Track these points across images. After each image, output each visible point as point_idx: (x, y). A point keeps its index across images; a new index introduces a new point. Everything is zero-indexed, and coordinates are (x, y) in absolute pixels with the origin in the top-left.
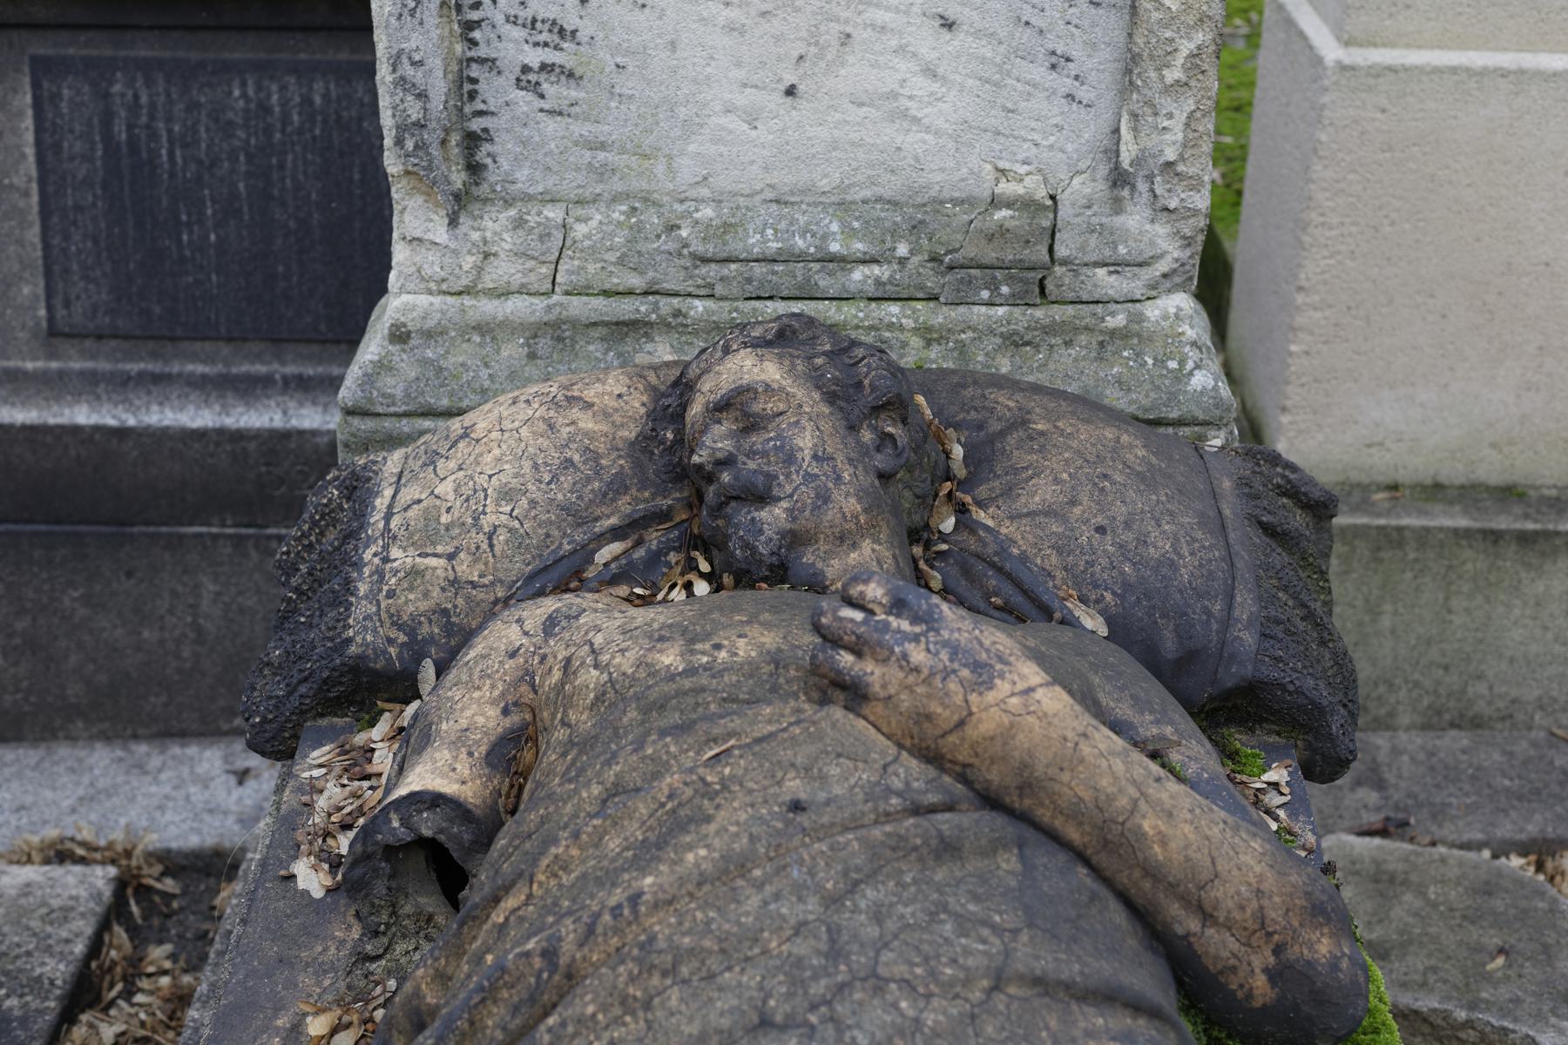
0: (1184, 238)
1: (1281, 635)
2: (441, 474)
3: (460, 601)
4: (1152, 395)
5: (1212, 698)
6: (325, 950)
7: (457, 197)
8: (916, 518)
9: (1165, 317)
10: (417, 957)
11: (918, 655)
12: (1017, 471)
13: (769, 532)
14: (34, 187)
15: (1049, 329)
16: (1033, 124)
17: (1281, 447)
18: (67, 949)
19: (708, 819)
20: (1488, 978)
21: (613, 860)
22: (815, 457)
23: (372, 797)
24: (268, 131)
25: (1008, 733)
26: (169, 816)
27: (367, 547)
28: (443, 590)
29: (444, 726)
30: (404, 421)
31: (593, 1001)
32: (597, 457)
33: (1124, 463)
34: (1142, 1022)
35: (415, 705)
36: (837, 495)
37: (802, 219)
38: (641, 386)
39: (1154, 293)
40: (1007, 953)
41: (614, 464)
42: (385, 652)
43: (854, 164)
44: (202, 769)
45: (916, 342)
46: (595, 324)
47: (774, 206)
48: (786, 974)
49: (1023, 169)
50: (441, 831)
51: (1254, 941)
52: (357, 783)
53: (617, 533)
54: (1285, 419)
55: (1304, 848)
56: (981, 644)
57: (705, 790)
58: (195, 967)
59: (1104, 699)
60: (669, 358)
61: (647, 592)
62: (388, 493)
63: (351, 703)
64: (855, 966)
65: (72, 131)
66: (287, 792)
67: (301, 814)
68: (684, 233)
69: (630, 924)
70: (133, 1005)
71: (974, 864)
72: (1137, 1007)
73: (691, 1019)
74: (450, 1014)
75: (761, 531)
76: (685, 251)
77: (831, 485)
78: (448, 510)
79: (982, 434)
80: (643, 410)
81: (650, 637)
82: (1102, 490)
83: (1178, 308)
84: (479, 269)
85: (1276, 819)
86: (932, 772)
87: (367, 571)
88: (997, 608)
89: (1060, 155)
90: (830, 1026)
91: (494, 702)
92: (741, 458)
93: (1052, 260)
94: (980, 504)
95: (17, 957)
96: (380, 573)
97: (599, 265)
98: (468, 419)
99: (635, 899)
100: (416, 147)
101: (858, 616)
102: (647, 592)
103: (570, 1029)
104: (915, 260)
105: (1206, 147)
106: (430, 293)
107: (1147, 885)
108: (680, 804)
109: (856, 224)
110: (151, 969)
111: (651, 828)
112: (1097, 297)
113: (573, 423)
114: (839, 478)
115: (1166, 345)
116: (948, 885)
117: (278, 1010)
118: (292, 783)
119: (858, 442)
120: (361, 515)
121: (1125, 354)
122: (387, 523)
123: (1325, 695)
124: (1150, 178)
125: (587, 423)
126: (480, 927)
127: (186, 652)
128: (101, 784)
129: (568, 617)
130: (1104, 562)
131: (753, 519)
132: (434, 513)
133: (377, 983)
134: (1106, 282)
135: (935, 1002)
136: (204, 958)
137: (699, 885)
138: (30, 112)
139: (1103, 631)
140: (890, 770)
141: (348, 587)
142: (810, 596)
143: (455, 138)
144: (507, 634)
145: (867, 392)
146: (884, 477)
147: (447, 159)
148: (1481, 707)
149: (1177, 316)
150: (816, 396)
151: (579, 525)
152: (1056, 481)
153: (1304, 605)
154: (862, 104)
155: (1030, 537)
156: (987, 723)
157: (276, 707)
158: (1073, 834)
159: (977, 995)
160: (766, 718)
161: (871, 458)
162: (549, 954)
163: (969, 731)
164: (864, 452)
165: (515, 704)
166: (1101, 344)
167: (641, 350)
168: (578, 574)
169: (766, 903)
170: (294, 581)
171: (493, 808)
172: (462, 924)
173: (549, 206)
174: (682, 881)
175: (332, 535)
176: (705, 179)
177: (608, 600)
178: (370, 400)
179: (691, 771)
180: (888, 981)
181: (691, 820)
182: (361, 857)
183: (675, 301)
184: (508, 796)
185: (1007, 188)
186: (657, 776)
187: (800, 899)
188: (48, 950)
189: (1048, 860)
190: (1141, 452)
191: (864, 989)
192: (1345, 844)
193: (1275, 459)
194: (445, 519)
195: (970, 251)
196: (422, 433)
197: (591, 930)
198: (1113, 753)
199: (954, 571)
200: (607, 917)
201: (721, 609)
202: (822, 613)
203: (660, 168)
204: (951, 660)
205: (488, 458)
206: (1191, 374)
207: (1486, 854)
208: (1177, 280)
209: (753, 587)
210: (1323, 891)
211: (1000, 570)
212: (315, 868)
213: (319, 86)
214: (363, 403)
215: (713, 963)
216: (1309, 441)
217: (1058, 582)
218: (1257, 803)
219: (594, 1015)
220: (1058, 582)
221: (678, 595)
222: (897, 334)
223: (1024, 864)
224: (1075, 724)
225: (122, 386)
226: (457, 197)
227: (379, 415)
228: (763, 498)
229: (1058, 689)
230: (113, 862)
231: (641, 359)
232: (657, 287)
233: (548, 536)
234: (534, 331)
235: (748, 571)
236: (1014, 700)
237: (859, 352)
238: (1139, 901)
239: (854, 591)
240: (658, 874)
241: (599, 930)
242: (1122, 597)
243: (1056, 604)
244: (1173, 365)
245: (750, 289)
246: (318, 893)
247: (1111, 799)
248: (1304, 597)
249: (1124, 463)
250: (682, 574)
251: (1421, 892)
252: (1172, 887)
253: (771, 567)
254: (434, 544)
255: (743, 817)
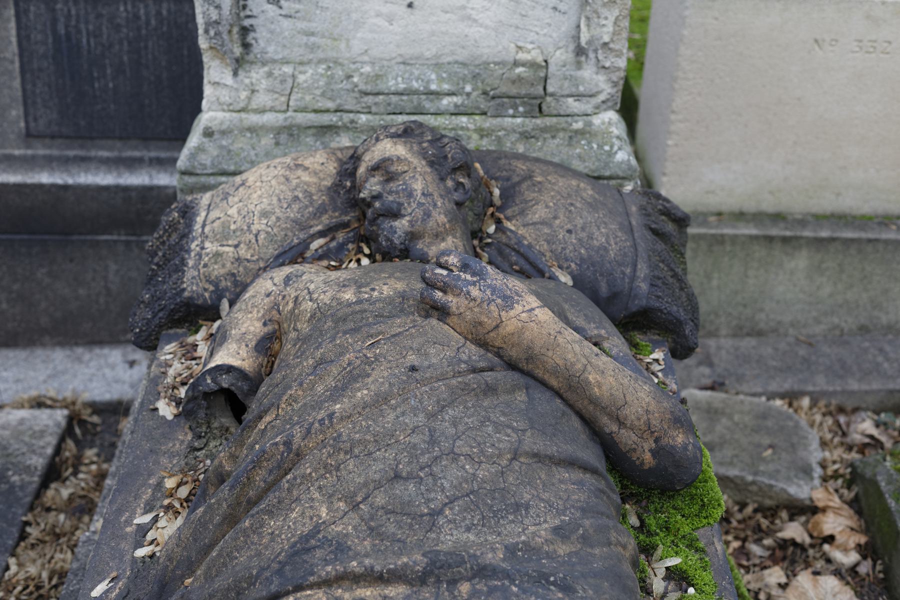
0: (613, 82)
1: (660, 285)
2: (231, 204)
3: (241, 269)
4: (597, 164)
5: (625, 317)
6: (174, 445)
7: (237, 60)
8: (475, 226)
9: (603, 123)
10: (221, 448)
11: (475, 292)
12: (526, 202)
13: (399, 232)
14: (17, 59)
15: (544, 130)
16: (536, 23)
17: (663, 193)
18: (43, 451)
19: (368, 375)
20: (764, 460)
21: (320, 397)
22: (423, 194)
23: (197, 369)
24: (139, 29)
25: (521, 331)
26: (94, 384)
27: (193, 241)
28: (232, 263)
29: (233, 332)
30: (211, 178)
31: (310, 467)
32: (311, 195)
33: (582, 198)
34: (588, 475)
35: (218, 323)
36: (435, 214)
37: (416, 73)
38: (333, 159)
39: (597, 111)
40: (520, 441)
41: (320, 199)
42: (203, 295)
43: (444, 44)
44: (111, 360)
45: (475, 136)
46: (310, 127)
47: (402, 66)
48: (408, 452)
49: (530, 46)
50: (232, 385)
51: (645, 436)
52: (189, 362)
53: (321, 234)
54: (665, 179)
55: (671, 391)
56: (507, 286)
57: (367, 361)
58: (109, 460)
59: (570, 316)
60: (348, 144)
61: (337, 264)
62: (203, 214)
63: (186, 321)
64: (443, 448)
65: (36, 29)
66: (153, 367)
67: (160, 377)
68: (355, 80)
69: (328, 428)
70: (77, 479)
71: (504, 398)
72: (586, 468)
73: (360, 475)
74: (237, 474)
75: (395, 232)
76: (356, 89)
77: (431, 208)
78: (235, 222)
79: (509, 183)
80: (334, 171)
81: (339, 285)
82: (570, 211)
83: (610, 120)
84: (249, 99)
85: (657, 377)
86: (482, 352)
87: (193, 254)
88: (517, 271)
89: (550, 39)
90: (430, 477)
91: (258, 319)
92: (385, 195)
93: (546, 94)
94: (508, 219)
95: (17, 456)
96: (199, 255)
97: (312, 96)
98: (244, 176)
99: (331, 416)
100: (216, 34)
101: (445, 272)
102: (337, 264)
103: (298, 481)
104: (475, 94)
105: (625, 35)
106: (224, 110)
107: (591, 408)
108: (354, 368)
109: (444, 75)
110: (87, 461)
111: (339, 380)
112: (568, 113)
113: (299, 178)
114: (435, 205)
115: (603, 138)
116: (490, 408)
117: (150, 475)
118: (156, 362)
119: (445, 186)
120: (189, 226)
121: (583, 142)
122: (203, 230)
123: (682, 315)
124: (596, 51)
125: (306, 177)
126: (252, 432)
127: (102, 300)
128: (60, 368)
129: (297, 276)
130: (571, 248)
131: (391, 226)
132: (227, 224)
133: (201, 462)
134: (573, 105)
135: (483, 466)
136: (113, 455)
137: (363, 408)
138: (13, 19)
139: (570, 283)
140: (461, 350)
141: (183, 262)
142: (421, 264)
143: (235, 30)
144: (266, 285)
145: (450, 162)
146: (459, 204)
147: (232, 41)
148: (762, 325)
149: (609, 123)
150: (424, 163)
151: (302, 230)
152: (547, 207)
153: (672, 270)
154: (447, 12)
155: (533, 235)
156: (510, 326)
157: (147, 324)
158: (554, 383)
159: (505, 462)
160: (397, 325)
161: (452, 195)
162: (288, 444)
163: (501, 330)
164: (448, 191)
165: (270, 320)
166: (571, 138)
167: (334, 141)
168: (302, 255)
169: (398, 417)
170: (156, 260)
171: (259, 373)
172: (243, 430)
173: (285, 65)
174: (355, 406)
175: (174, 237)
176: (366, 51)
177: (317, 267)
178: (194, 167)
179: (359, 351)
180: (459, 455)
181: (359, 376)
182: (191, 399)
183: (351, 115)
184: (266, 367)
185: (522, 56)
186: (342, 354)
187: (415, 415)
188: (34, 452)
189: (541, 395)
190: (590, 192)
191: (447, 459)
192: (693, 394)
193: (658, 196)
194: (233, 227)
195: (503, 89)
196: (220, 184)
197: (308, 431)
198: (574, 341)
199: (494, 253)
200: (317, 425)
201: (375, 271)
202: (426, 271)
203: (343, 46)
204: (492, 295)
205: (255, 196)
206: (616, 153)
207: (764, 399)
208: (610, 104)
209: (391, 261)
210: (680, 411)
211: (518, 252)
212: (168, 404)
213: (165, 5)
214: (190, 169)
215: (371, 447)
216: (679, 189)
217: (548, 258)
218: (647, 369)
219: (310, 474)
220: (548, 258)
221: (353, 265)
222: (466, 132)
223: (529, 397)
224: (555, 326)
225: (65, 163)
226: (237, 60)
227: (197, 175)
228: (396, 214)
229: (546, 309)
230: (66, 407)
231: (333, 145)
232: (341, 108)
233: (286, 235)
234: (278, 131)
235: (389, 253)
236: (524, 315)
237: (446, 140)
238: (587, 416)
239: (442, 260)
240: (342, 403)
241: (313, 431)
242: (580, 265)
243: (547, 269)
244: (607, 148)
245: (390, 109)
246: (170, 417)
247: (573, 364)
248: (672, 265)
249: (582, 198)
250: (355, 255)
251: (730, 417)
252: (604, 409)
253: (401, 251)
254: (227, 240)
255: (386, 374)
